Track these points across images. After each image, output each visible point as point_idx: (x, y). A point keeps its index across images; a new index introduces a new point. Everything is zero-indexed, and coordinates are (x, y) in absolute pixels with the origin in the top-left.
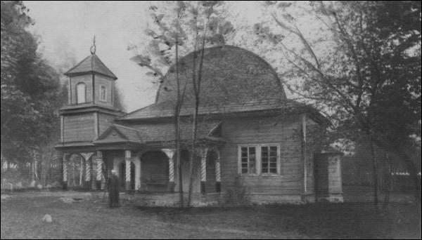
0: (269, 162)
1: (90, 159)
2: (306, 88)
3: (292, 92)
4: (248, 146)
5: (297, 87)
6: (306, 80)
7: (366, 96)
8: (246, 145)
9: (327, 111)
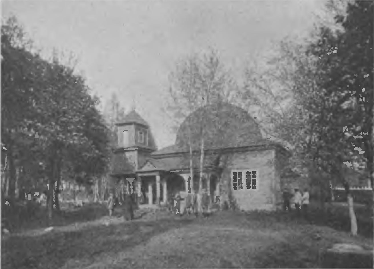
0: (252, 183)
1: (133, 183)
2: (276, 131)
3: (267, 133)
4: (251, 171)
5: (270, 130)
6: (58, 74)
7: (316, 136)
8: (236, 171)
9: (289, 146)
